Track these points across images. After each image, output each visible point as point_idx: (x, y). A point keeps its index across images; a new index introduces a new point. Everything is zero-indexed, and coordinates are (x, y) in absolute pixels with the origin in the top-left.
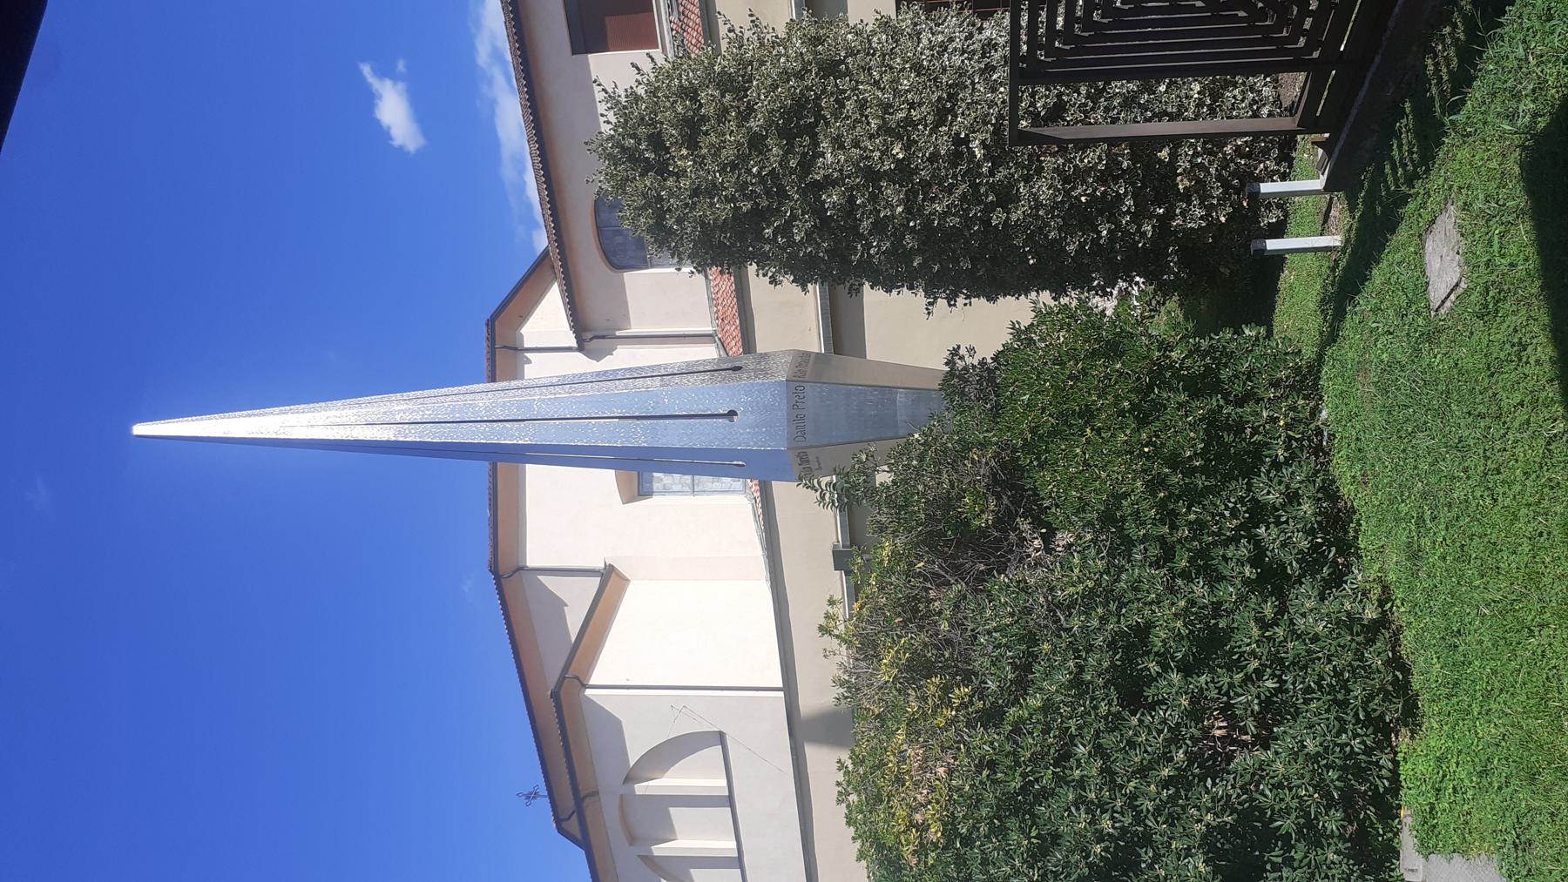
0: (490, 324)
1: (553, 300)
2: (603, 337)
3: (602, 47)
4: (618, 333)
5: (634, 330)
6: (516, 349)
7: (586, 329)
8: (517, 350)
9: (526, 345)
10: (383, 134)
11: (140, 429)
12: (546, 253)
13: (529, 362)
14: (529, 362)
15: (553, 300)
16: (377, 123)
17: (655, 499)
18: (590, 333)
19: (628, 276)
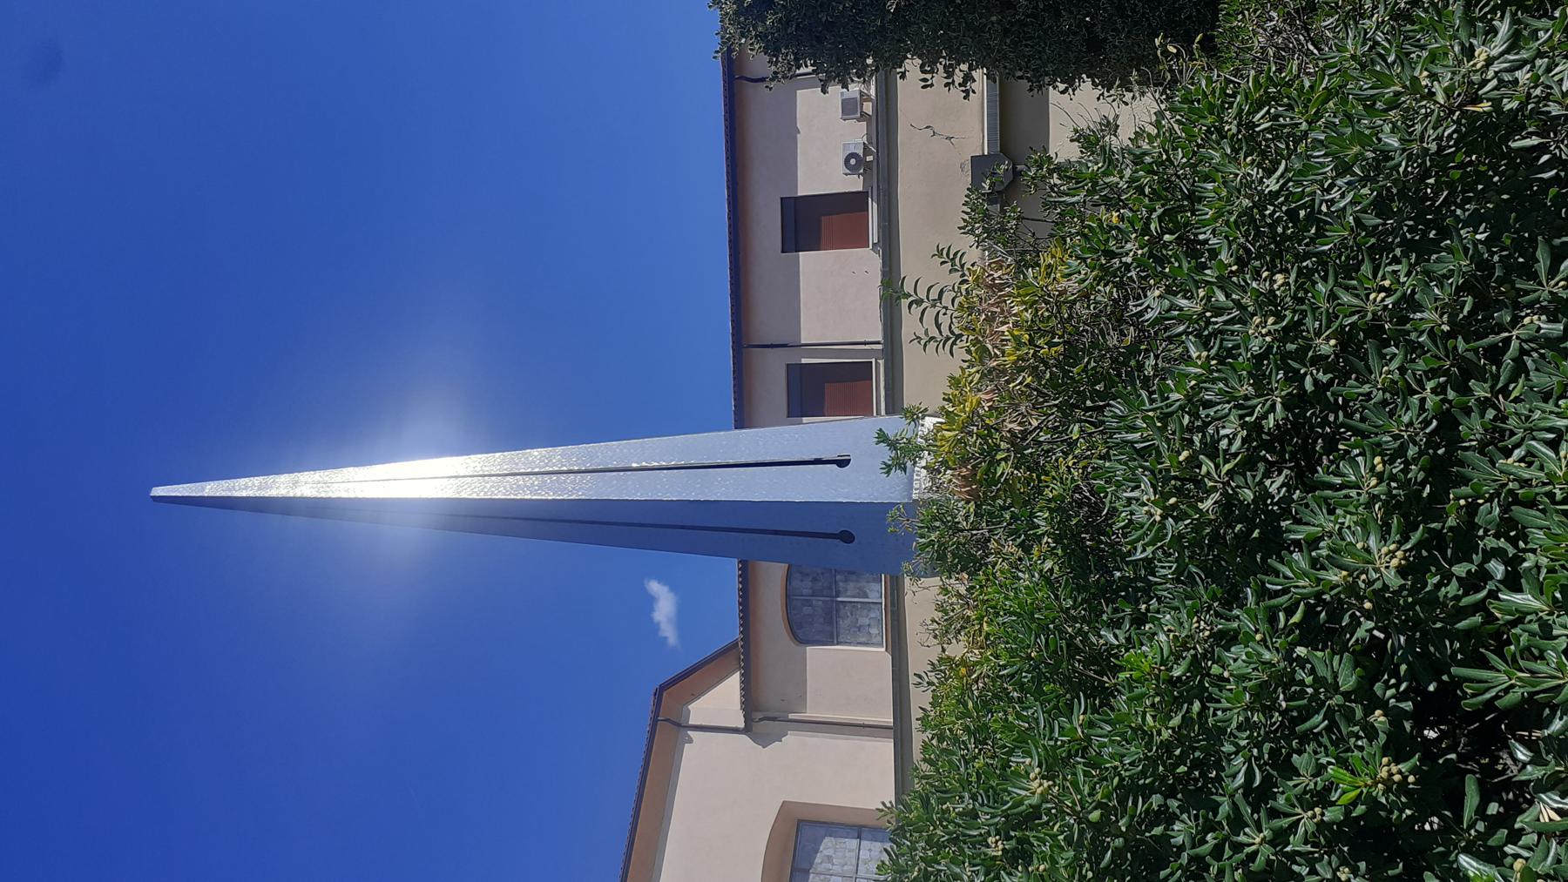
0: (659, 693)
1: (731, 686)
2: (774, 719)
3: (815, 246)
4: (791, 716)
5: (810, 714)
6: (679, 725)
7: (757, 709)
8: (681, 726)
9: (691, 722)
10: (655, 627)
11: (158, 491)
12: (735, 644)
13: (691, 741)
14: (691, 741)
15: (731, 686)
16: (651, 620)
17: (792, 739)
18: (762, 718)
19: (811, 650)
